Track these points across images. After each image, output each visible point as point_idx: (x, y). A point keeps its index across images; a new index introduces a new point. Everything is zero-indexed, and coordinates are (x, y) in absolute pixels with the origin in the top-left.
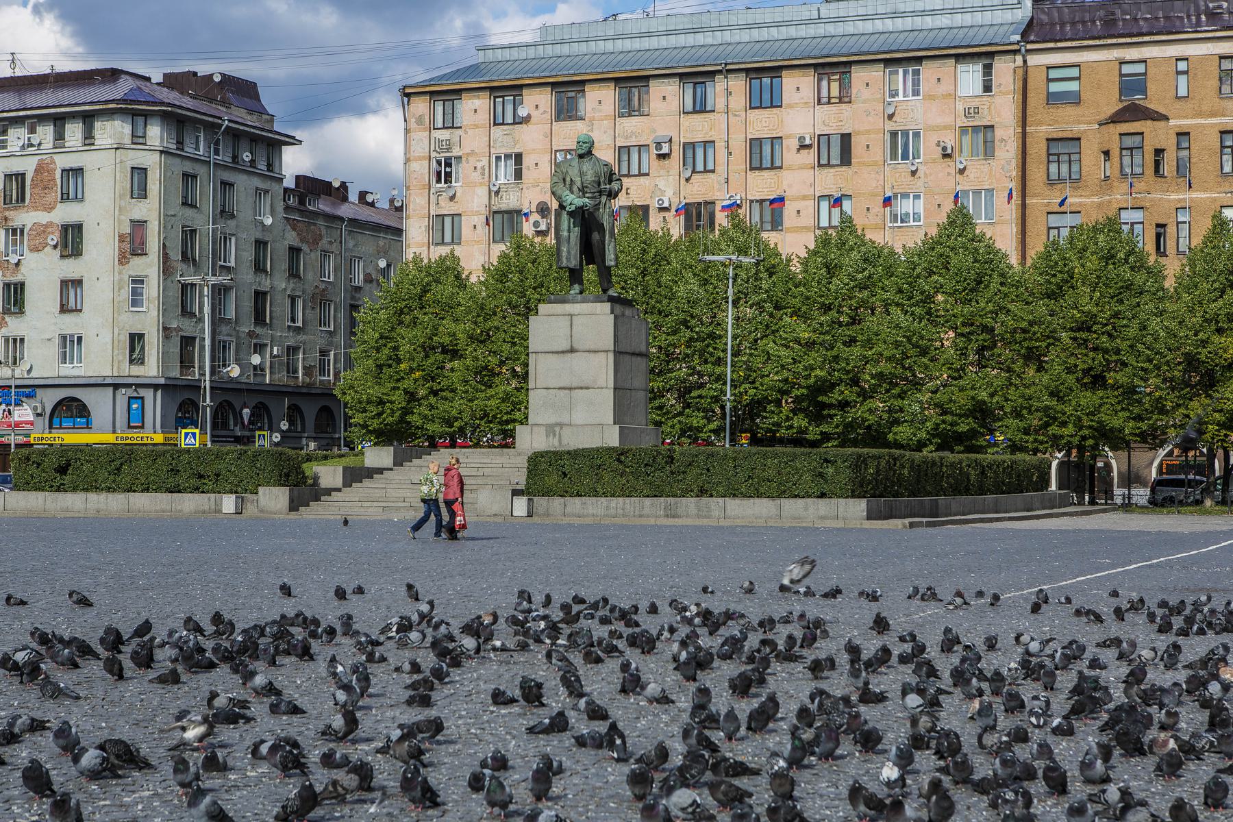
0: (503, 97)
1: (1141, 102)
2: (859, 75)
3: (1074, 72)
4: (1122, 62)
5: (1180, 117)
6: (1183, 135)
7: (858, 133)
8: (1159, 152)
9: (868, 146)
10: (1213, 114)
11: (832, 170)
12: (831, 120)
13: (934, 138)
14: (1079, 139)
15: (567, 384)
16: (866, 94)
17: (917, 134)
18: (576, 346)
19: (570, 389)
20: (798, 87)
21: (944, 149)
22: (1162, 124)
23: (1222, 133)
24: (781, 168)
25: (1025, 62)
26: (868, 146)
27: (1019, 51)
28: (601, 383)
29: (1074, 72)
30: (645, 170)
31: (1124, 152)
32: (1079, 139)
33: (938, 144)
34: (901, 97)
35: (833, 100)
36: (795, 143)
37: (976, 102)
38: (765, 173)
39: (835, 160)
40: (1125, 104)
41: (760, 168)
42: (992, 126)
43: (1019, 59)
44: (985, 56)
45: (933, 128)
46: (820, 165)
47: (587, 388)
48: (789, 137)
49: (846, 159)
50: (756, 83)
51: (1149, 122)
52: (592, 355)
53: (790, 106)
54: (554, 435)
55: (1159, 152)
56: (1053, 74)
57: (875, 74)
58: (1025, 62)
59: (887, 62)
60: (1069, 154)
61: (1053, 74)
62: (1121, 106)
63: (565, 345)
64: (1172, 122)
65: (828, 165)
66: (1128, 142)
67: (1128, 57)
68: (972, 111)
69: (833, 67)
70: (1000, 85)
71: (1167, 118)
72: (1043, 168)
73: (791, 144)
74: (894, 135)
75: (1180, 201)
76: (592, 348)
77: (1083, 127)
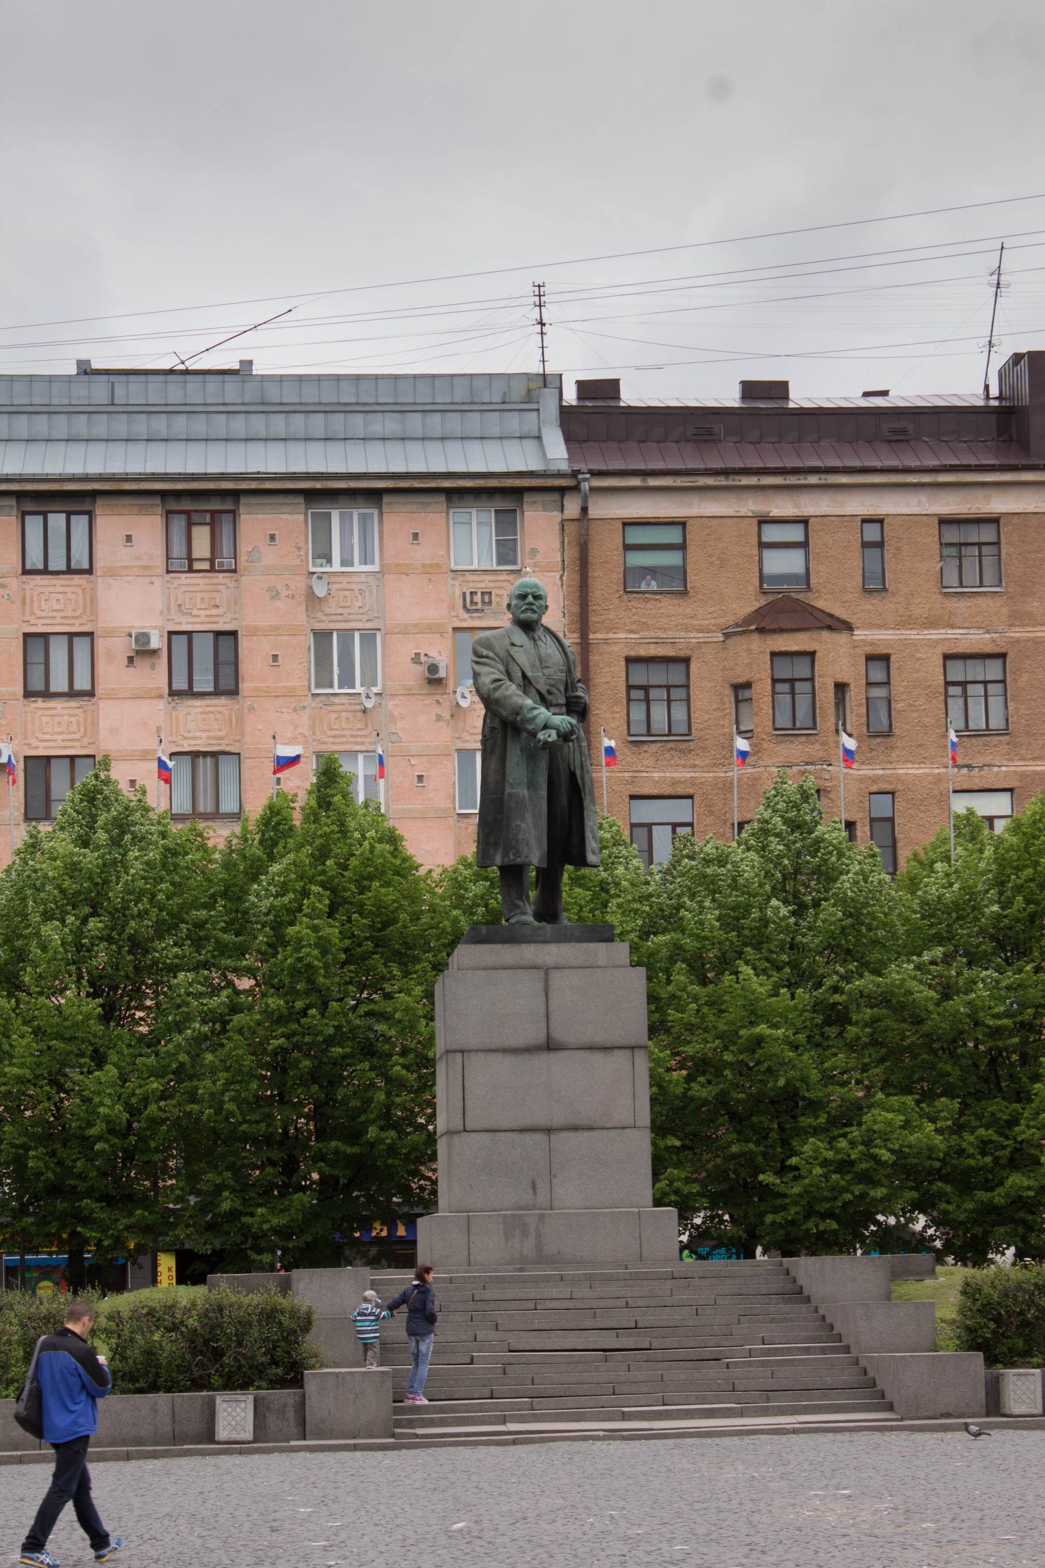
0: (45, 514)
1: (801, 597)
2: (254, 524)
3: (673, 536)
4: (764, 521)
5: (871, 626)
6: (879, 659)
7: (255, 632)
8: (841, 688)
9: (275, 658)
10: (931, 623)
11: (197, 703)
12: (203, 604)
13: (407, 648)
14: (686, 661)
15: (544, 1121)
16: (270, 556)
17: (369, 639)
18: (559, 1034)
19: (549, 1131)
20: (129, 540)
21: (433, 668)
22: (842, 638)
23: (947, 657)
24: (91, 694)
25: (584, 510)
26: (275, 658)
27: (576, 489)
28: (621, 1115)
29: (673, 536)
30: (82, 683)
31: (780, 687)
32: (686, 661)
33: (416, 659)
34: (336, 566)
35: (197, 566)
36: (121, 647)
37: (486, 583)
38: (58, 705)
39: (204, 682)
40: (771, 598)
41: (47, 694)
42: (234, 634)
43: (572, 507)
44: (504, 495)
45: (405, 630)
46: (172, 693)
47: (590, 1128)
48: (110, 633)
49: (227, 687)
50: (34, 524)
51: (826, 634)
52: (598, 1057)
53: (113, 573)
54: (525, 1234)
55: (841, 688)
56: (637, 536)
57: (292, 521)
58: (584, 510)
59: (311, 496)
60: (668, 687)
61: (637, 536)
62: (763, 601)
63: (538, 1036)
64: (859, 634)
65: (190, 693)
66: (785, 671)
67: (776, 512)
68: (478, 598)
69: (201, 506)
70: (534, 552)
71: (848, 627)
72: (621, 709)
73: (113, 650)
74: (322, 637)
75: (875, 780)
76: (600, 1038)
77: (695, 637)
